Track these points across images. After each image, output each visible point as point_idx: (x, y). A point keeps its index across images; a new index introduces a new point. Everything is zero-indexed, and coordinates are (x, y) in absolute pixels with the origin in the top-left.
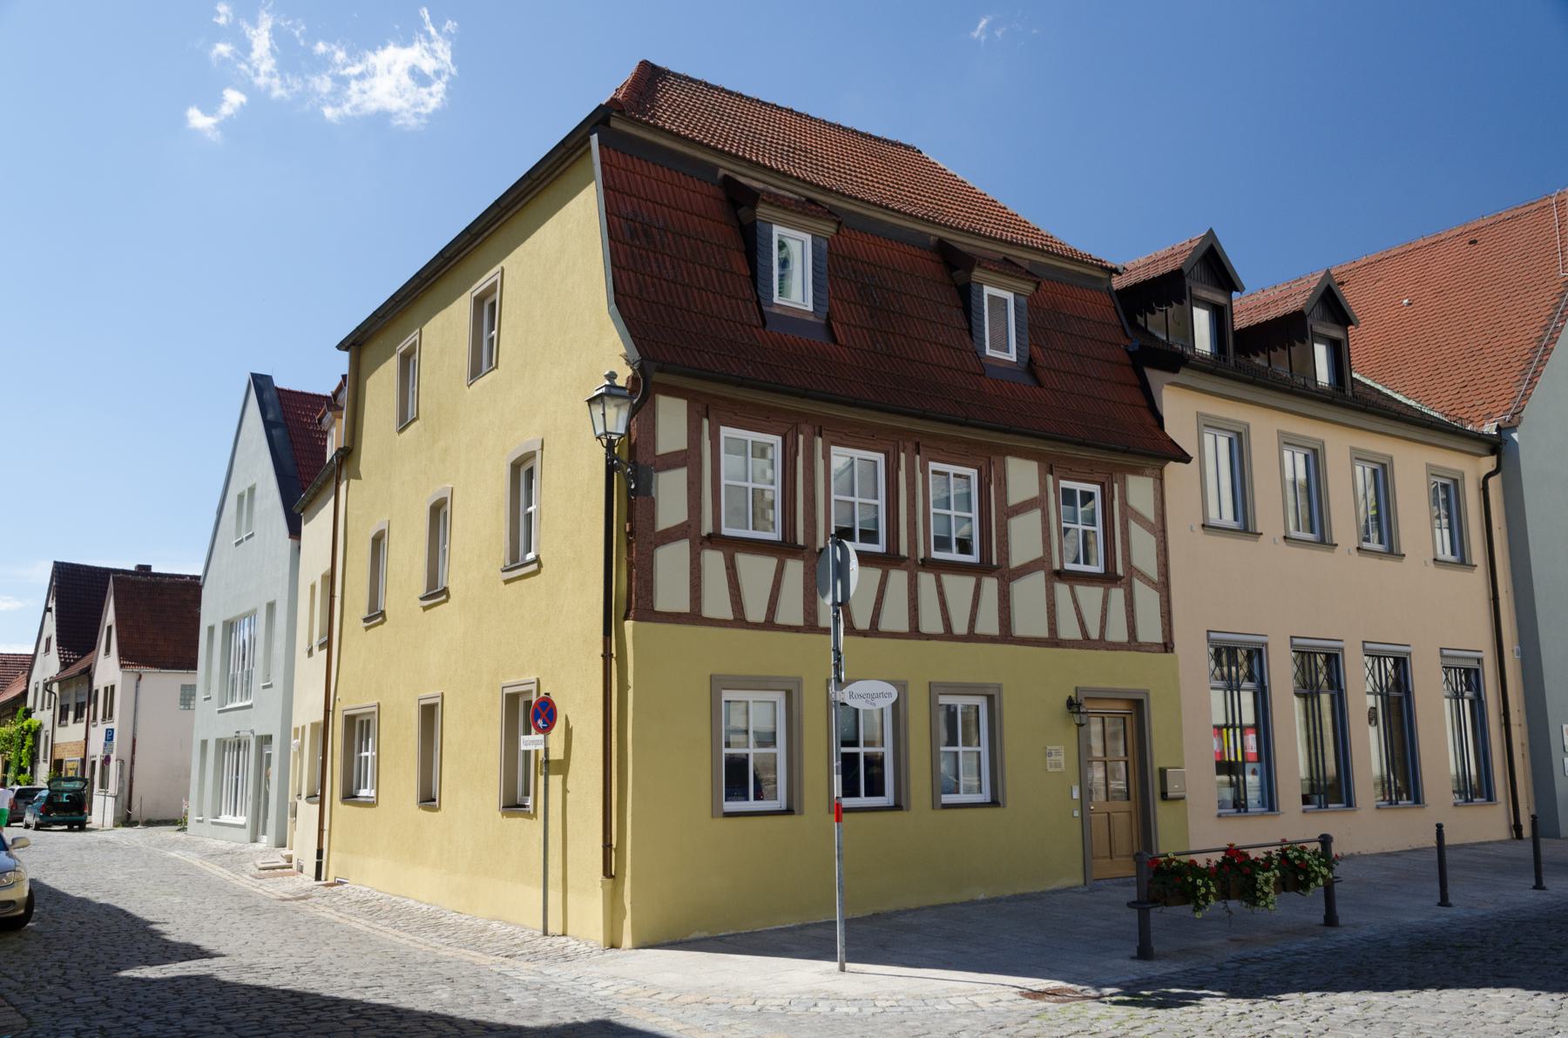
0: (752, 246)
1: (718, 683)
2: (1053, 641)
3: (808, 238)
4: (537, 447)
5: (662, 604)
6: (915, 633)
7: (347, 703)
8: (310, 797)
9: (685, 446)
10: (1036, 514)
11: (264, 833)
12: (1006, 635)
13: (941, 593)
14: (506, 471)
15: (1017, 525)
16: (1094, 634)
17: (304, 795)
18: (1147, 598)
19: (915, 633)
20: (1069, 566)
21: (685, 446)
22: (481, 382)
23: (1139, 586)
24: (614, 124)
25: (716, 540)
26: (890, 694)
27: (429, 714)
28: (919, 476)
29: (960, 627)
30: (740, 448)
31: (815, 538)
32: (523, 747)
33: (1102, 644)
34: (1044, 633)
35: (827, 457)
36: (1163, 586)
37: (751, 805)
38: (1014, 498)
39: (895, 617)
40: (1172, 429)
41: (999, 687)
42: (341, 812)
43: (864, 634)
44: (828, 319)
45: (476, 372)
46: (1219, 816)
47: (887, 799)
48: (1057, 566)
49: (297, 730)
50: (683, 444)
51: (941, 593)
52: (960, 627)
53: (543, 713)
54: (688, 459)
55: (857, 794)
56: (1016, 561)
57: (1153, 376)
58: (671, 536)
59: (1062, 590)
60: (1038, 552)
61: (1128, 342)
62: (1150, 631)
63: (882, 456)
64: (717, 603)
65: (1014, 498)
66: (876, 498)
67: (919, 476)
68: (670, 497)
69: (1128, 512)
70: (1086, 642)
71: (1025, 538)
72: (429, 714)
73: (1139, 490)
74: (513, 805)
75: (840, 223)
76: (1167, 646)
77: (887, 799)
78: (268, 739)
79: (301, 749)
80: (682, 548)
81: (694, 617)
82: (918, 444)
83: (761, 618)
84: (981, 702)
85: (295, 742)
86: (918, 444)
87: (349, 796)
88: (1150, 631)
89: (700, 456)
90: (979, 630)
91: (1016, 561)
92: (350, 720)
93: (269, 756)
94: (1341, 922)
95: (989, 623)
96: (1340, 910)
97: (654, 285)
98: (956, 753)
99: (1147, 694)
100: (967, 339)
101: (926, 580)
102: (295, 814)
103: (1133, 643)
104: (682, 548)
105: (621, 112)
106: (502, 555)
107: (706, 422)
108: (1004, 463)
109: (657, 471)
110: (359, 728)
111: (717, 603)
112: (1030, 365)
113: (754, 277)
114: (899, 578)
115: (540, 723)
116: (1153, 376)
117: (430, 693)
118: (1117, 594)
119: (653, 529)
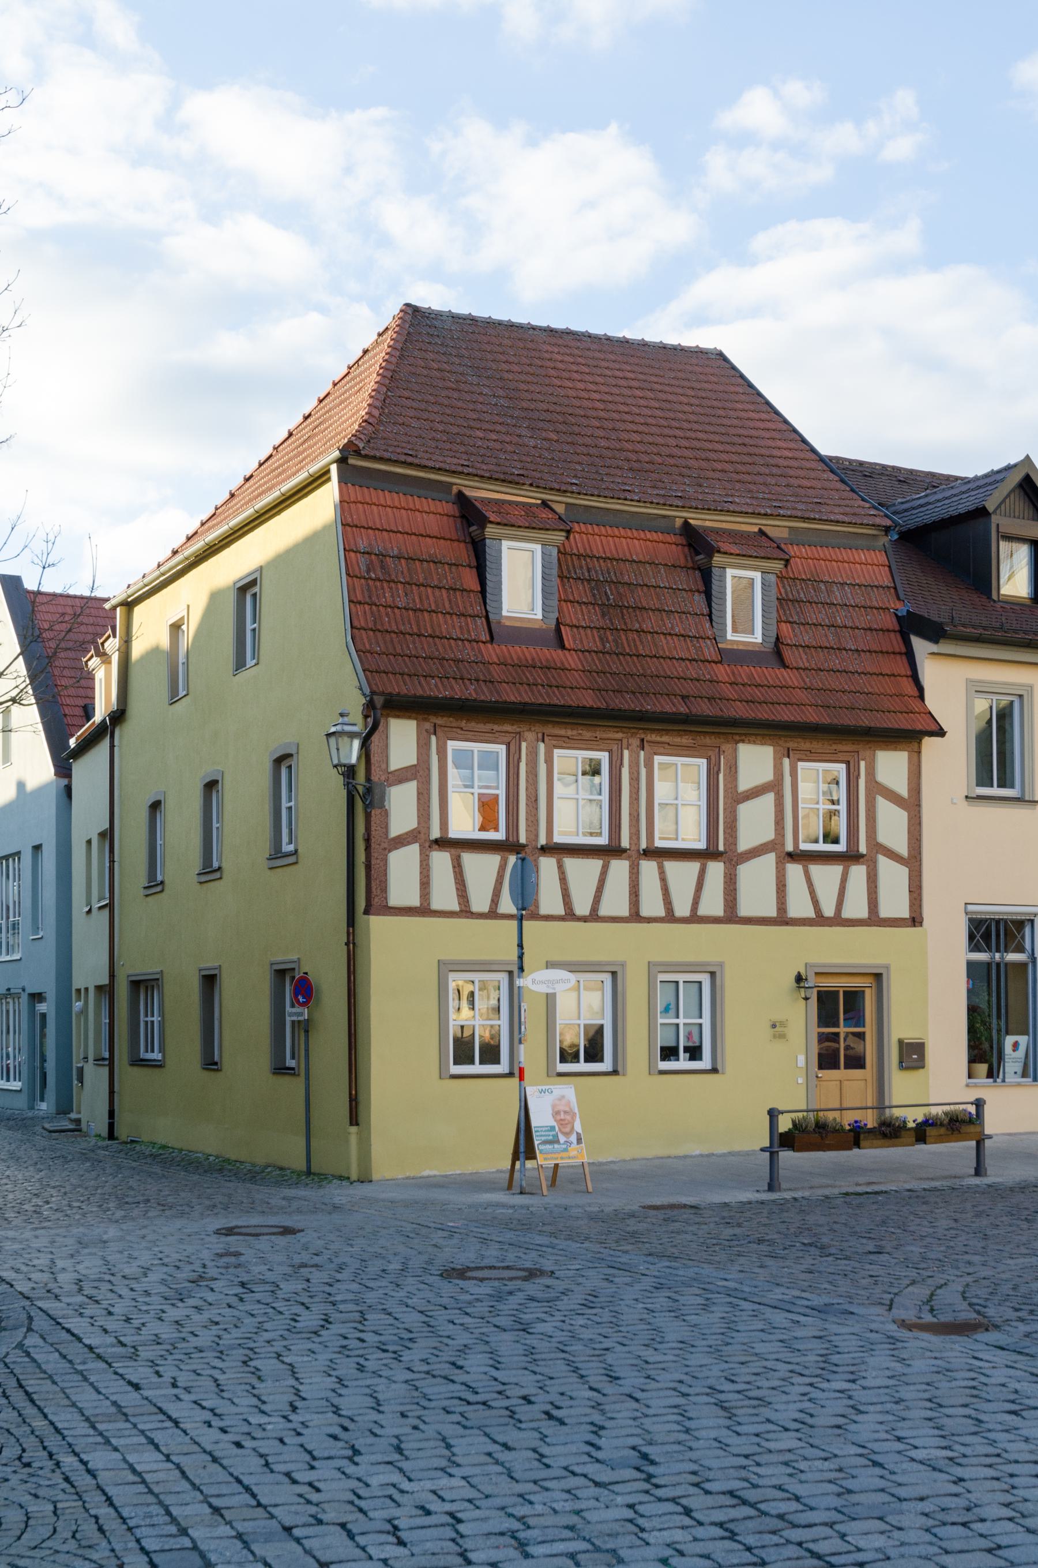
0: (481, 563)
1: (446, 968)
2: (782, 919)
3: (538, 548)
4: (293, 752)
5: (395, 899)
6: (636, 916)
7: (132, 966)
8: (99, 1060)
9: (415, 762)
10: (769, 798)
11: (42, 1100)
12: (731, 916)
13: (663, 880)
14: (268, 766)
15: (746, 811)
16: (829, 911)
17: (91, 1058)
18: (893, 878)
19: (636, 916)
20: (804, 846)
21: (415, 762)
22: (244, 675)
23: (884, 863)
24: (351, 461)
25: (444, 843)
26: (569, 981)
27: (210, 981)
28: (643, 771)
29: (682, 909)
30: (464, 762)
31: (537, 836)
32: (20, 1084)
33: (838, 921)
34: (773, 913)
35: (549, 761)
36: (913, 861)
37: (477, 1068)
38: (744, 784)
39: (615, 903)
40: (932, 702)
41: (721, 965)
42: (130, 1077)
43: (584, 919)
44: (558, 623)
45: (240, 664)
46: (967, 1086)
47: (606, 1065)
48: (789, 847)
49: (78, 991)
50: (413, 760)
51: (663, 880)
52: (682, 909)
53: (305, 989)
54: (418, 772)
55: (472, 1062)
56: (744, 844)
57: (920, 646)
58: (401, 842)
59: (794, 871)
60: (770, 835)
61: (899, 605)
62: (894, 902)
63: (606, 754)
64: (444, 897)
65: (744, 784)
66: (600, 794)
67: (643, 771)
68: (401, 808)
69: (876, 789)
70: (820, 920)
71: (755, 823)
72: (210, 981)
73: (891, 766)
74: (280, 1069)
75: (568, 532)
76: (915, 920)
77: (606, 1065)
78: (37, 997)
79: (84, 1011)
80: (413, 850)
81: (424, 910)
82: (642, 740)
83: (485, 908)
84: (705, 979)
85: (78, 1005)
86: (642, 740)
87: (138, 1062)
88: (894, 902)
89: (429, 769)
90: (702, 911)
91: (744, 844)
92: (136, 985)
93: (44, 1016)
94: (988, 1173)
95: (713, 904)
96: (988, 1162)
97: (387, 615)
98: (677, 1025)
99: (887, 967)
100: (708, 625)
101: (649, 868)
102: (81, 1080)
103: (874, 919)
104: (413, 850)
105: (358, 453)
106: (265, 848)
107: (433, 738)
108: (735, 750)
109: (390, 785)
110: (144, 986)
111: (444, 897)
112: (777, 651)
113: (483, 592)
114: (620, 868)
115: (301, 1000)
116: (920, 646)
117: (209, 963)
118: (858, 873)
119: (387, 833)
